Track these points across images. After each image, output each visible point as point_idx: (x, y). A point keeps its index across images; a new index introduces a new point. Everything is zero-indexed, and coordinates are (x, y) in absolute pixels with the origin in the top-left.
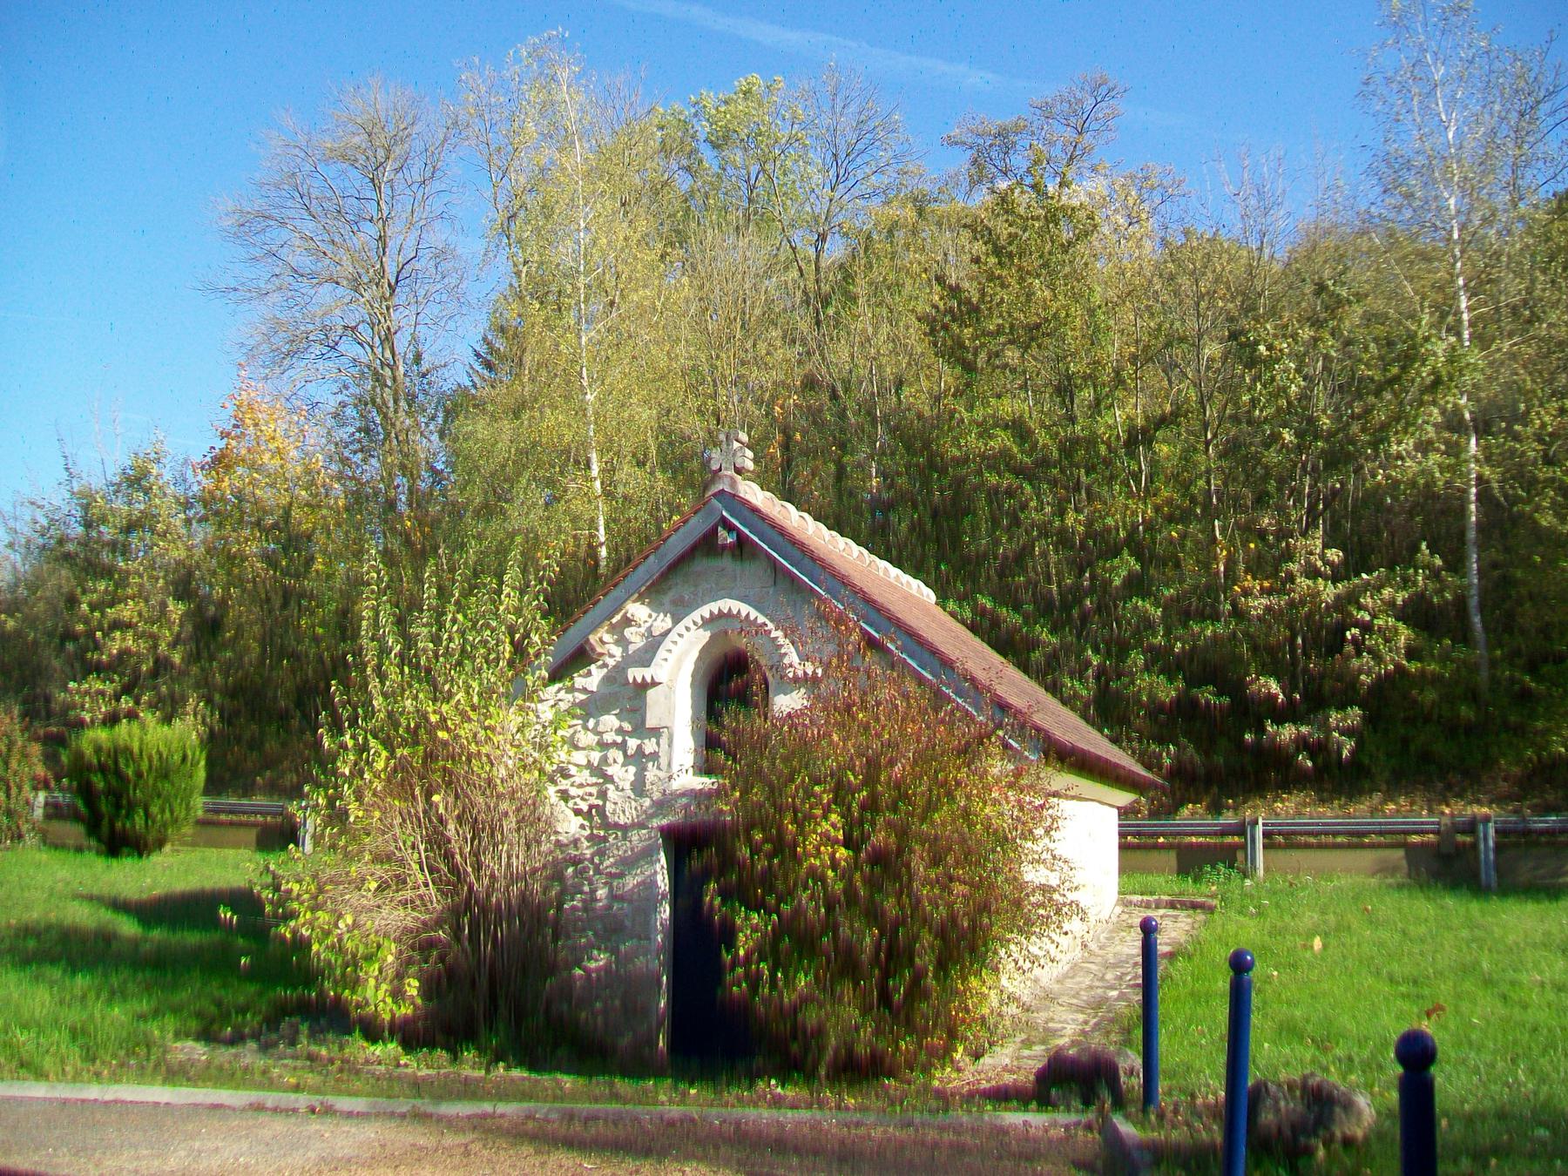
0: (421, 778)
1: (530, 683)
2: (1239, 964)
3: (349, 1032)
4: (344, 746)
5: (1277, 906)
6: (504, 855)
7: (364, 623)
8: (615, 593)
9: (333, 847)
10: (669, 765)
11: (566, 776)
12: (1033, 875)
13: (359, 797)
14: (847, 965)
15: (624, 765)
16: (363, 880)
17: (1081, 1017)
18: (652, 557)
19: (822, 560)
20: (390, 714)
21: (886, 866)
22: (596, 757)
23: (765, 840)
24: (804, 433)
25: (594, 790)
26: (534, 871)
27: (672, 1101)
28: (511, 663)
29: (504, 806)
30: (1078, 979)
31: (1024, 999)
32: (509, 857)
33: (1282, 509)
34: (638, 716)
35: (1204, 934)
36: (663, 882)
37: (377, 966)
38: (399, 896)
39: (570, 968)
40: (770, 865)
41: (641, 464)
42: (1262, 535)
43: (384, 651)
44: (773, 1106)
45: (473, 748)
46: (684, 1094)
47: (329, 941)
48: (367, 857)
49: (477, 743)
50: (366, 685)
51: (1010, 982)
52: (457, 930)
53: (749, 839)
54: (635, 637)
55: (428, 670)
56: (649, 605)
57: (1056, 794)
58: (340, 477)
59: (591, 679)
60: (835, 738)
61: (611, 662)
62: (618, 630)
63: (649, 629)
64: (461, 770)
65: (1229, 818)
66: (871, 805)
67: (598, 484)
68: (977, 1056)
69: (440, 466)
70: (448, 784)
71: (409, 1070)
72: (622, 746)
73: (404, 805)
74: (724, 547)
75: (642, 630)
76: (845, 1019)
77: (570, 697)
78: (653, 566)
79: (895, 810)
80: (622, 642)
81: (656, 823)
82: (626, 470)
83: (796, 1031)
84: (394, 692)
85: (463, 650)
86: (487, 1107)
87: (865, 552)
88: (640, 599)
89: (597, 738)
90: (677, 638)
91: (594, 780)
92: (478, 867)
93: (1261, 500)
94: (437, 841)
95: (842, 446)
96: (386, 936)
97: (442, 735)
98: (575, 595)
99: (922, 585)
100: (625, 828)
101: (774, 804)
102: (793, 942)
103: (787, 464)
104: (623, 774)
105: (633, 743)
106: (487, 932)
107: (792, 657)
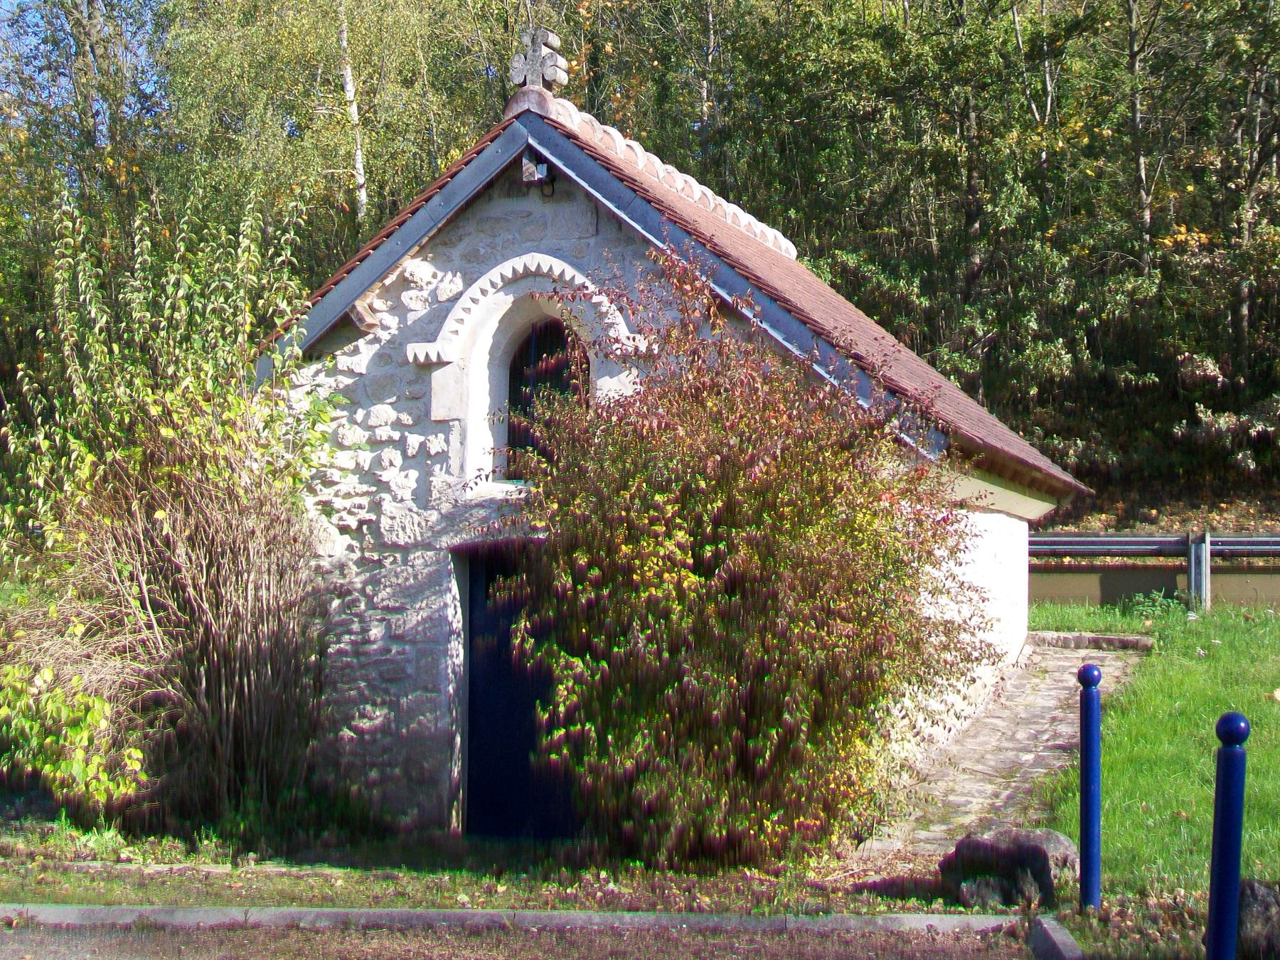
0: (141, 488)
1: (278, 364)
2: (1231, 731)
3: (53, 816)
4: (35, 448)
5: (1231, 645)
6: (251, 586)
7: (58, 287)
8: (389, 245)
9: (25, 580)
10: (462, 468)
11: (329, 483)
12: (928, 608)
13: (59, 515)
14: (693, 722)
15: (402, 469)
16: (67, 622)
17: (990, 788)
18: (436, 199)
19: (659, 202)
20: (97, 406)
21: (747, 594)
22: (366, 458)
23: (590, 565)
24: (616, 41)
25: (365, 501)
26: (290, 606)
27: (468, 895)
28: (252, 336)
29: (250, 523)
30: (981, 739)
31: (919, 766)
32: (257, 588)
33: (1227, 143)
34: (419, 404)
35: (1142, 683)
36: (456, 617)
37: (85, 734)
38: (117, 641)
39: (336, 726)
40: (598, 597)
41: (408, 83)
42: (1198, 175)
43: (87, 323)
44: (595, 902)
45: (208, 449)
46: (490, 891)
47: (21, 704)
48: (71, 592)
49: (211, 443)
50: (64, 368)
51: (905, 749)
52: (190, 682)
53: (572, 563)
54: (415, 302)
55: (144, 348)
56: (433, 261)
57: (962, 504)
58: (21, 102)
59: (359, 358)
60: (681, 432)
61: (385, 336)
62: (393, 294)
63: (434, 293)
64: (192, 477)
65: (1145, 534)
66: (728, 516)
67: (353, 110)
68: (859, 839)
69: (149, 90)
70: (176, 495)
71: (133, 867)
72: (401, 445)
73: (117, 524)
74: (530, 184)
75: (425, 294)
76: (691, 793)
77: (331, 381)
78: (439, 208)
79: (759, 522)
80: (399, 309)
81: (446, 541)
82: (391, 92)
83: (631, 806)
84: (100, 378)
85: (190, 322)
86: (236, 914)
87: (709, 192)
88: (422, 252)
89: (367, 434)
90: (470, 304)
91: (365, 488)
92: (217, 603)
93: (1198, 130)
94: (162, 569)
95: (664, 59)
96: (97, 692)
97: (166, 432)
98: (331, 249)
99: (779, 235)
100: (405, 549)
101: (604, 518)
102: (628, 694)
103: (596, 80)
104: (403, 481)
105: (414, 441)
106: (230, 683)
107: (621, 329)
